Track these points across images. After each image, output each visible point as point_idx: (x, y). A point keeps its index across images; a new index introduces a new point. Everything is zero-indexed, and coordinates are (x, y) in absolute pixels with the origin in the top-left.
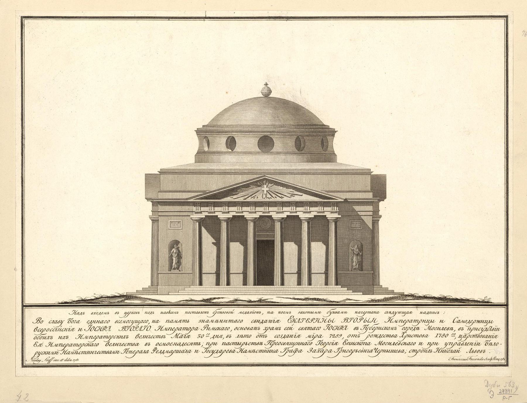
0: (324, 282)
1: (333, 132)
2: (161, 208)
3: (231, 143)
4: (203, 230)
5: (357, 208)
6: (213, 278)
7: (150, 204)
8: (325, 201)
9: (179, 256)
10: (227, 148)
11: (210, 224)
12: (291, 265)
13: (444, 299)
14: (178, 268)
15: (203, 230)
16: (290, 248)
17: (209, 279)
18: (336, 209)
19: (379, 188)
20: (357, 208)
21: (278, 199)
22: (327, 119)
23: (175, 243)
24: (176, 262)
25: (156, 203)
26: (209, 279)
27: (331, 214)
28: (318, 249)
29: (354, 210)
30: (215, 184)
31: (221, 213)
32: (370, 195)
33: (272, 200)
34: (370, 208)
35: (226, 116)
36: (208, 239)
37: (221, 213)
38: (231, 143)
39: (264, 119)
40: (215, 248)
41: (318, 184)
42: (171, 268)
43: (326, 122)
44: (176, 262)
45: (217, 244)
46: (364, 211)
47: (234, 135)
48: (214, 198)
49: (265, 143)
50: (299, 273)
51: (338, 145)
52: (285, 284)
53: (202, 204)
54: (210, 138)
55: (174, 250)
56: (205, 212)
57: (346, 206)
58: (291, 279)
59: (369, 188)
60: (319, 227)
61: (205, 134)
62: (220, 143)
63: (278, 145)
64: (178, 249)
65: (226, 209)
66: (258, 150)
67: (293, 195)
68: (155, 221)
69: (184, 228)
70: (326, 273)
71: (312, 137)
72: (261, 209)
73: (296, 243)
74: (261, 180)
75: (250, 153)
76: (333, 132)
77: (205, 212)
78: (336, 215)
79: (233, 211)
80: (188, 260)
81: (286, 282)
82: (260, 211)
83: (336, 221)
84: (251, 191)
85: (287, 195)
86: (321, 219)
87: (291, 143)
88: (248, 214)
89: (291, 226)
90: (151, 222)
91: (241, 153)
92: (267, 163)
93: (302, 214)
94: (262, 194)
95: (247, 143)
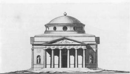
0: (74, 67)
1: (84, 25)
2: (35, 46)
3: (55, 29)
4: (47, 52)
5: (91, 46)
6: (81, 65)
7: (31, 45)
8: (82, 44)
9: (40, 60)
10: (54, 29)
11: (49, 51)
12: (72, 62)
13: (117, 71)
14: (39, 63)
15: (47, 52)
16: (72, 57)
17: (48, 66)
18: (85, 46)
19: (98, 40)
20: (91, 46)
21: (68, 44)
22: (82, 21)
23: (38, 56)
24: (39, 62)
25: (33, 45)
26: (48, 66)
27: (84, 47)
28: (80, 57)
29: (90, 47)
30: (49, 40)
31: (52, 48)
32: (95, 43)
33: (67, 44)
34: (95, 46)
35: (52, 21)
36: (48, 55)
37: (52, 48)
38: (55, 29)
39: (65, 21)
40: (50, 57)
41: (81, 39)
42: (37, 63)
43: (82, 23)
44: (39, 62)
45: (51, 56)
46: (93, 47)
47: (56, 26)
48: (51, 43)
49: (65, 28)
50: (75, 64)
51: (85, 29)
52: (55, 67)
53: (46, 45)
54: (49, 27)
55: (38, 58)
56: (48, 47)
57: (88, 46)
58: (72, 66)
59: (95, 41)
60: (80, 52)
61: (47, 26)
62: (51, 28)
63: (69, 29)
64: (39, 58)
65: (53, 47)
66: (63, 30)
67: (73, 43)
68: (33, 50)
69: (41, 52)
70: (82, 64)
71: (79, 27)
72: (56, 46)
73: (74, 56)
74: (64, 38)
75: (72, 31)
76: (84, 25)
77: (48, 47)
78: (86, 48)
79: (56, 47)
80: (42, 61)
81: (71, 67)
82: (63, 47)
83: (85, 50)
84: (60, 42)
85: (71, 42)
86: (81, 50)
87: (72, 29)
88: (60, 48)
89: (72, 52)
90: (31, 50)
91: (69, 31)
92: (65, 34)
93: (75, 47)
94: (64, 42)
95: (60, 28)
